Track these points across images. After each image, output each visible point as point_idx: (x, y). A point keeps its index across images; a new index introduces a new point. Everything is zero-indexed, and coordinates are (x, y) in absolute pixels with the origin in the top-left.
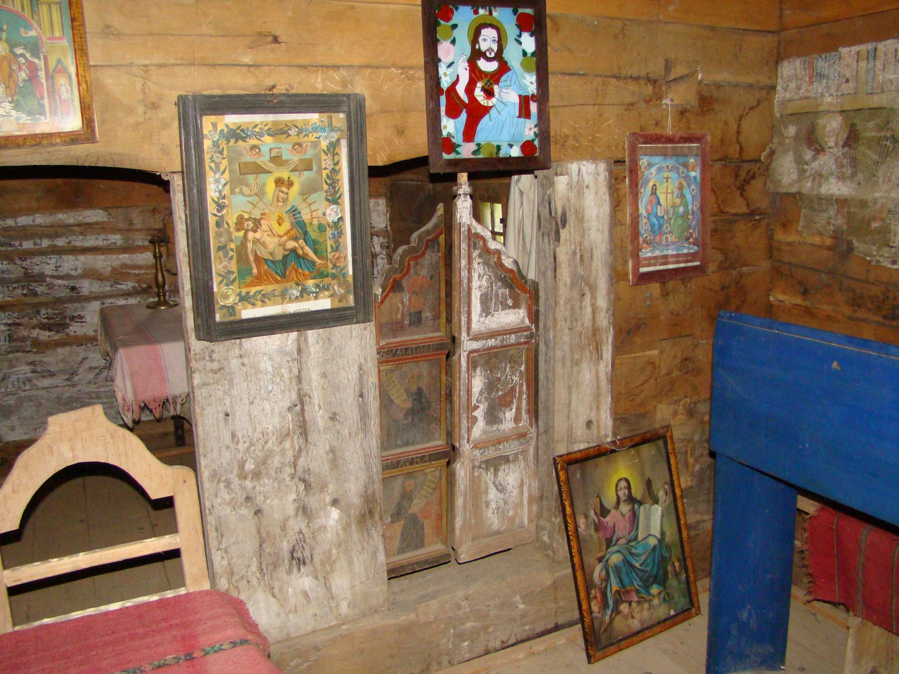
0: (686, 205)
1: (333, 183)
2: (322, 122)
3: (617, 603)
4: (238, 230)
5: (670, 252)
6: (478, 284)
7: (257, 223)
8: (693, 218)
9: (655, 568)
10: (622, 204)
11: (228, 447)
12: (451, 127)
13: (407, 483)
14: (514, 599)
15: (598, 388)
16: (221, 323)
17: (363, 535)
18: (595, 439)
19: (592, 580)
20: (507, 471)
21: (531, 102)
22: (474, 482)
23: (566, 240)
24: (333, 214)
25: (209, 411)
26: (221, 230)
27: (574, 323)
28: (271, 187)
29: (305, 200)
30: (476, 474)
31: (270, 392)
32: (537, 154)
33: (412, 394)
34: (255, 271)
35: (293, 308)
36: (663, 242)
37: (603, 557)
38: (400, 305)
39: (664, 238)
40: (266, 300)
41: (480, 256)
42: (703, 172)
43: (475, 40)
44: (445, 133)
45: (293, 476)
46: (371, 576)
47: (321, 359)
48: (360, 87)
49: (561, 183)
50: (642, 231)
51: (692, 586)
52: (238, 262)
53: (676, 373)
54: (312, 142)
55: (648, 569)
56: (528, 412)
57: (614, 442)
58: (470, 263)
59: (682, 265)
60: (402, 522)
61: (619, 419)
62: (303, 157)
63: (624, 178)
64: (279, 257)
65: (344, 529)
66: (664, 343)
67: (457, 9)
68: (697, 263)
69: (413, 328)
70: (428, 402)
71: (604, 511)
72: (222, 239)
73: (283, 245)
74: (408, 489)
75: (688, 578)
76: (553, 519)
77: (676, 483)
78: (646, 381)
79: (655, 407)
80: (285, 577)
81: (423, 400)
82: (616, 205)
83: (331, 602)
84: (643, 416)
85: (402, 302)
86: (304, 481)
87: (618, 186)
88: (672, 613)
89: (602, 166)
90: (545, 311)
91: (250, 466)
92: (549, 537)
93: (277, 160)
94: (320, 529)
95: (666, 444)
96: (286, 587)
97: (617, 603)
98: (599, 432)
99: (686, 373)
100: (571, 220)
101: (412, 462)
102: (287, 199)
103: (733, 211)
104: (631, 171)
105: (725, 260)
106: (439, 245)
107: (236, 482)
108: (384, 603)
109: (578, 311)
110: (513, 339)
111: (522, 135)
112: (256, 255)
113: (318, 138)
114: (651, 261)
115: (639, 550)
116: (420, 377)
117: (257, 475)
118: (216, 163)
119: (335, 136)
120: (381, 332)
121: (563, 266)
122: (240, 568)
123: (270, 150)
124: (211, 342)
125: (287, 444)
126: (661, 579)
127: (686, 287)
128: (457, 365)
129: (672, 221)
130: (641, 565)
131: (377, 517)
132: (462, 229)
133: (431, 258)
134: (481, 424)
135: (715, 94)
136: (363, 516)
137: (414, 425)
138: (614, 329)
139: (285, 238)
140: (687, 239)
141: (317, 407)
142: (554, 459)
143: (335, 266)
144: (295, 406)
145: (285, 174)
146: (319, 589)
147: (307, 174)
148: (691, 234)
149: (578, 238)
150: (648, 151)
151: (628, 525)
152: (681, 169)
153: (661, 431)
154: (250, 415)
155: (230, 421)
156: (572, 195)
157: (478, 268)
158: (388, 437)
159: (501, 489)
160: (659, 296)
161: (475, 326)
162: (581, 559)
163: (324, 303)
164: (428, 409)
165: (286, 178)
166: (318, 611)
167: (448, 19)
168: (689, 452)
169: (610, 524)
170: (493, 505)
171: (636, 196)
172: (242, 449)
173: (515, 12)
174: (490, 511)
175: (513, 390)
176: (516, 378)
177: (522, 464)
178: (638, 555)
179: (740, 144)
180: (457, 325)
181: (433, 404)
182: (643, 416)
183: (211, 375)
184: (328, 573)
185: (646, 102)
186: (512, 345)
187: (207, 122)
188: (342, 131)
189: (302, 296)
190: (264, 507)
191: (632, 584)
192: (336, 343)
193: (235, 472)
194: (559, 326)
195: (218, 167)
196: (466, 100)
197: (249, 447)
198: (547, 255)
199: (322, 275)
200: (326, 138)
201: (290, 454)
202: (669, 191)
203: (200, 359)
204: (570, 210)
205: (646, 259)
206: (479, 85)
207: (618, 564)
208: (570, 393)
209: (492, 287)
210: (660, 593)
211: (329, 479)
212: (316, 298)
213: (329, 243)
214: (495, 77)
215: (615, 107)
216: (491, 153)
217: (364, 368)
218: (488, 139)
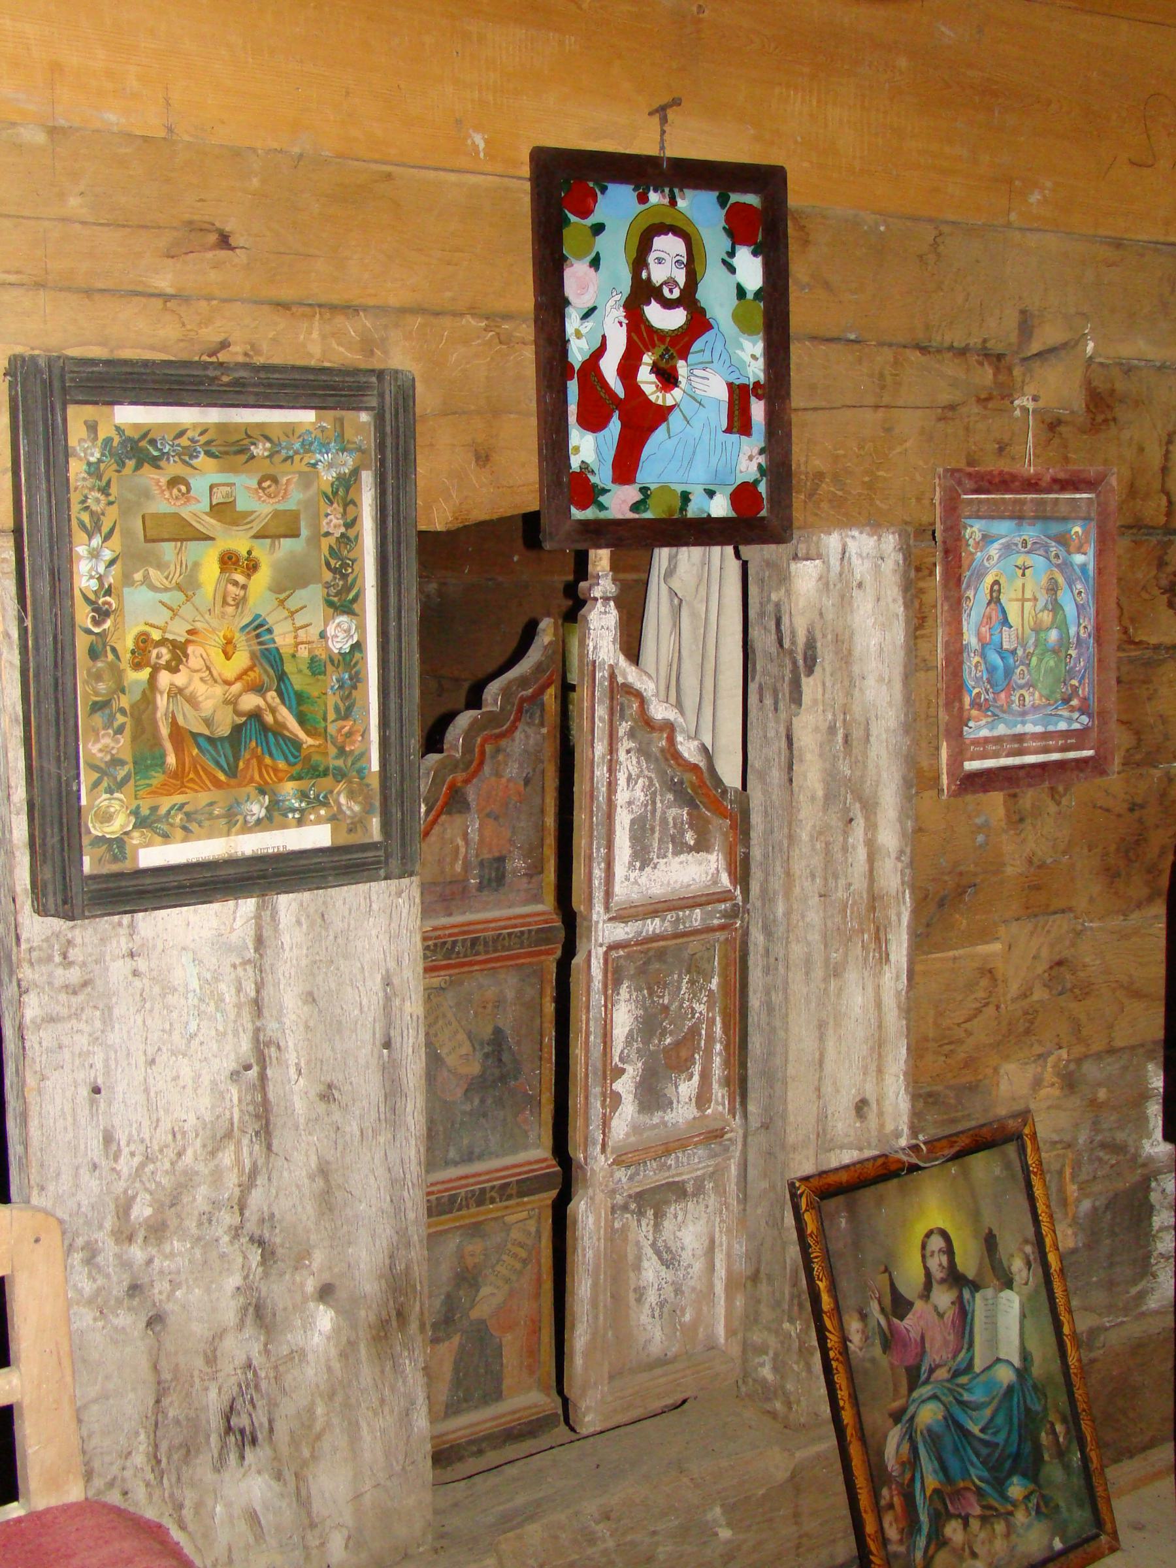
0: (1063, 626)
1: (341, 565)
2: (323, 429)
3: (939, 1519)
4: (137, 666)
5: (1030, 728)
7: (179, 653)
8: (1080, 655)
9: (1015, 1437)
10: (929, 622)
11: (95, 1167)
12: (588, 449)
13: (470, 1248)
14: (709, 1517)
15: (880, 1027)
16: (93, 877)
17: (383, 1372)
18: (874, 1142)
19: (882, 1466)
21: (753, 399)
22: (615, 1239)
23: (815, 702)
24: (341, 635)
25: (56, 1081)
26: (99, 664)
28: (210, 571)
29: (282, 603)
30: (617, 1225)
31: (192, 1037)
32: (763, 513)
33: (482, 1045)
34: (171, 759)
35: (249, 844)
36: (1015, 707)
37: (903, 1410)
38: (460, 842)
39: (1015, 698)
40: (193, 826)
41: (631, 734)
42: (1100, 554)
43: (639, 263)
44: (575, 463)
45: (236, 1232)
46: (398, 1468)
47: (304, 962)
48: (399, 357)
49: (806, 576)
50: (970, 683)
51: (1096, 1481)
52: (134, 738)
53: (1039, 994)
54: (301, 473)
55: (1001, 1438)
56: (727, 1082)
57: (915, 1148)
58: (612, 750)
59: (1055, 756)
60: (456, 1339)
61: (924, 1098)
62: (281, 507)
63: (935, 570)
64: (224, 730)
65: (343, 1355)
66: (1014, 927)
67: (604, 190)
68: (1090, 753)
71: (899, 1305)
72: (101, 686)
73: (233, 702)
75: (1085, 1459)
76: (786, 1325)
77: (1048, 1241)
78: (979, 1011)
79: (996, 1070)
80: (210, 1477)
81: (506, 1057)
82: (918, 622)
84: (973, 1088)
85: (465, 836)
86: (261, 1243)
87: (921, 584)
88: (1058, 1545)
89: (890, 541)
90: (766, 856)
91: (142, 1211)
92: (775, 1369)
93: (223, 511)
94: (290, 1356)
95: (1022, 1150)
96: (210, 1503)
97: (939, 1519)
99: (1060, 994)
100: (826, 657)
101: (481, 1198)
102: (244, 599)
103: (1153, 640)
104: (947, 552)
105: (1137, 747)
106: (543, 710)
107: (109, 1249)
110: (696, 918)
111: (733, 470)
112: (174, 724)
113: (314, 465)
114: (987, 746)
115: (976, 1396)
116: (499, 1003)
117: (157, 1231)
118: (92, 513)
119: (348, 462)
120: (441, 895)
121: (808, 756)
122: (107, 1459)
123: (211, 488)
124: (72, 919)
125: (227, 1157)
126: (1028, 1463)
127: (1059, 804)
128: (583, 977)
129: (1034, 660)
130: (982, 1430)
131: (414, 1326)
132: (598, 675)
133: (530, 739)
134: (628, 1110)
135: (1120, 386)
136: (384, 1324)
137: (485, 1115)
138: (912, 893)
139: (237, 687)
140: (1066, 700)
141: (292, 1071)
142: (792, 1185)
143: (342, 752)
144: (248, 1067)
145: (240, 544)
147: (286, 543)
148: (1075, 689)
149: (840, 699)
150: (984, 508)
151: (951, 1338)
152: (1054, 548)
153: (1012, 1124)
154: (147, 1091)
155: (102, 1105)
157: (628, 763)
158: (439, 1138)
159: (668, 1258)
160: (1003, 824)
161: (620, 890)
162: (858, 1415)
163: (316, 836)
164: (516, 1079)
165: (243, 553)
167: (585, 213)
168: (1068, 1171)
169: (914, 1335)
171: (956, 605)
172: (125, 1171)
173: (723, 201)
174: (646, 1310)
175: (694, 1032)
176: (701, 1007)
177: (712, 1200)
178: (977, 1407)
179: (1168, 494)
180: (585, 886)
182: (973, 1088)
183: (63, 997)
184: (305, 1464)
185: (983, 401)
186: (696, 932)
187: (77, 417)
188: (363, 452)
189: (269, 817)
190: (169, 1307)
191: (966, 1474)
192: (338, 925)
193: (108, 1225)
194: (797, 890)
195: (97, 527)
196: (620, 391)
197: (142, 1165)
198: (771, 734)
199: (314, 771)
200: (330, 465)
201: (232, 1180)
202: (1028, 595)
203: (40, 961)
204: (824, 636)
205: (976, 742)
206: (648, 359)
207: (937, 1429)
208: (822, 1038)
209: (654, 803)
210: (1027, 1497)
212: (300, 823)
213: (332, 700)
214: (681, 343)
215: (919, 412)
216: (671, 511)
217: (396, 981)
218: (665, 479)
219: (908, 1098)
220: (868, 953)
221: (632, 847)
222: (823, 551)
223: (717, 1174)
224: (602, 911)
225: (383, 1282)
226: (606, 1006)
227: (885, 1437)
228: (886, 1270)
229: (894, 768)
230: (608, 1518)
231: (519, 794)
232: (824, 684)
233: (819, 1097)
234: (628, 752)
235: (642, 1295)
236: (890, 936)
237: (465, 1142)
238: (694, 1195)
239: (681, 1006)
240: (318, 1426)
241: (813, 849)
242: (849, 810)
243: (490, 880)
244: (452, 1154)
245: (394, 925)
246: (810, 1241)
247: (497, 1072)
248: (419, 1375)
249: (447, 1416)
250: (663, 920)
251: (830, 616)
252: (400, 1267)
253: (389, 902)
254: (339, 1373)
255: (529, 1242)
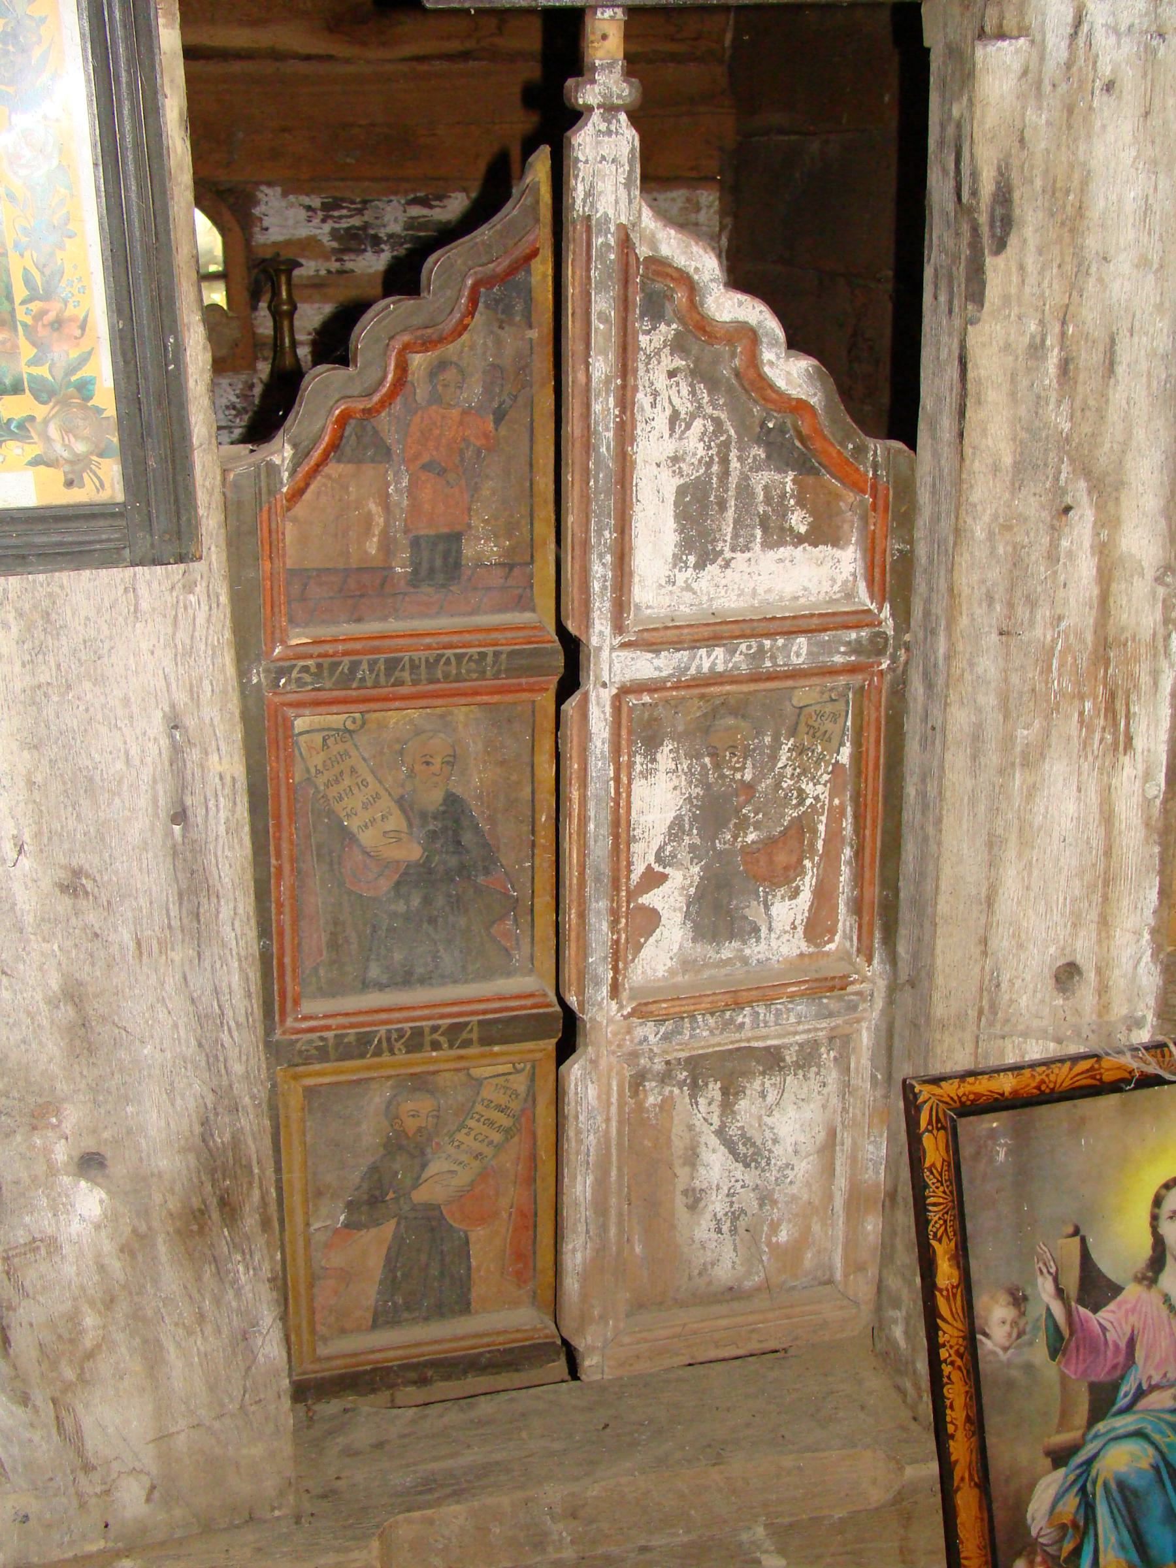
6: (669, 447)
13: (410, 1105)
15: (1108, 852)
17: (199, 1279)
20: (771, 1097)
23: (1006, 299)
27: (1022, 612)
37: (1075, 1449)
38: (373, 507)
41: (678, 346)
46: (232, 1407)
56: (857, 907)
58: (625, 368)
65: (126, 1250)
69: (427, 591)
70: (486, 845)
71: (1094, 1287)
74: (411, 1125)
81: (467, 838)
83: (82, 1479)
94: (32, 1245)
98: (1104, 1008)
101: (415, 1041)
108: (281, 1494)
109: (1042, 570)
110: (800, 651)
131: (250, 1221)
137: (432, 921)
146: (37, 1436)
149: (1056, 295)
156: (1039, 120)
157: (663, 387)
159: (747, 1152)
164: (487, 871)
166: (33, 1506)
169: (1117, 1336)
170: (717, 1205)
175: (802, 827)
176: (816, 787)
177: (833, 1076)
181: (507, 858)
184: (68, 1387)
186: (796, 674)
194: (964, 621)
198: (944, 355)
207: (1134, 1481)
208: (993, 863)
209: (725, 461)
211: (62, 1087)
217: (190, 722)
219: (1156, 970)
220: (1091, 731)
221: (681, 530)
222: (1032, 20)
223: (843, 1042)
224: (608, 631)
225: (191, 1157)
226: (617, 779)
227: (1031, 1486)
228: (1076, 1232)
229: (1159, 423)
230: (574, 1516)
231: (486, 436)
232: (1021, 267)
233: (985, 953)
234: (672, 374)
235: (697, 1200)
236: (1135, 709)
237: (398, 956)
238: (798, 1066)
239: (778, 786)
240: (88, 1342)
241: (993, 552)
242: (1064, 492)
243: (432, 570)
244: (374, 972)
245: (182, 636)
246: (930, 1180)
247: (453, 861)
248: (264, 1290)
249: (375, 1326)
250: (732, 652)
251: (1040, 144)
252: (221, 1138)
253: (170, 599)
254: (120, 1275)
255: (515, 1106)
